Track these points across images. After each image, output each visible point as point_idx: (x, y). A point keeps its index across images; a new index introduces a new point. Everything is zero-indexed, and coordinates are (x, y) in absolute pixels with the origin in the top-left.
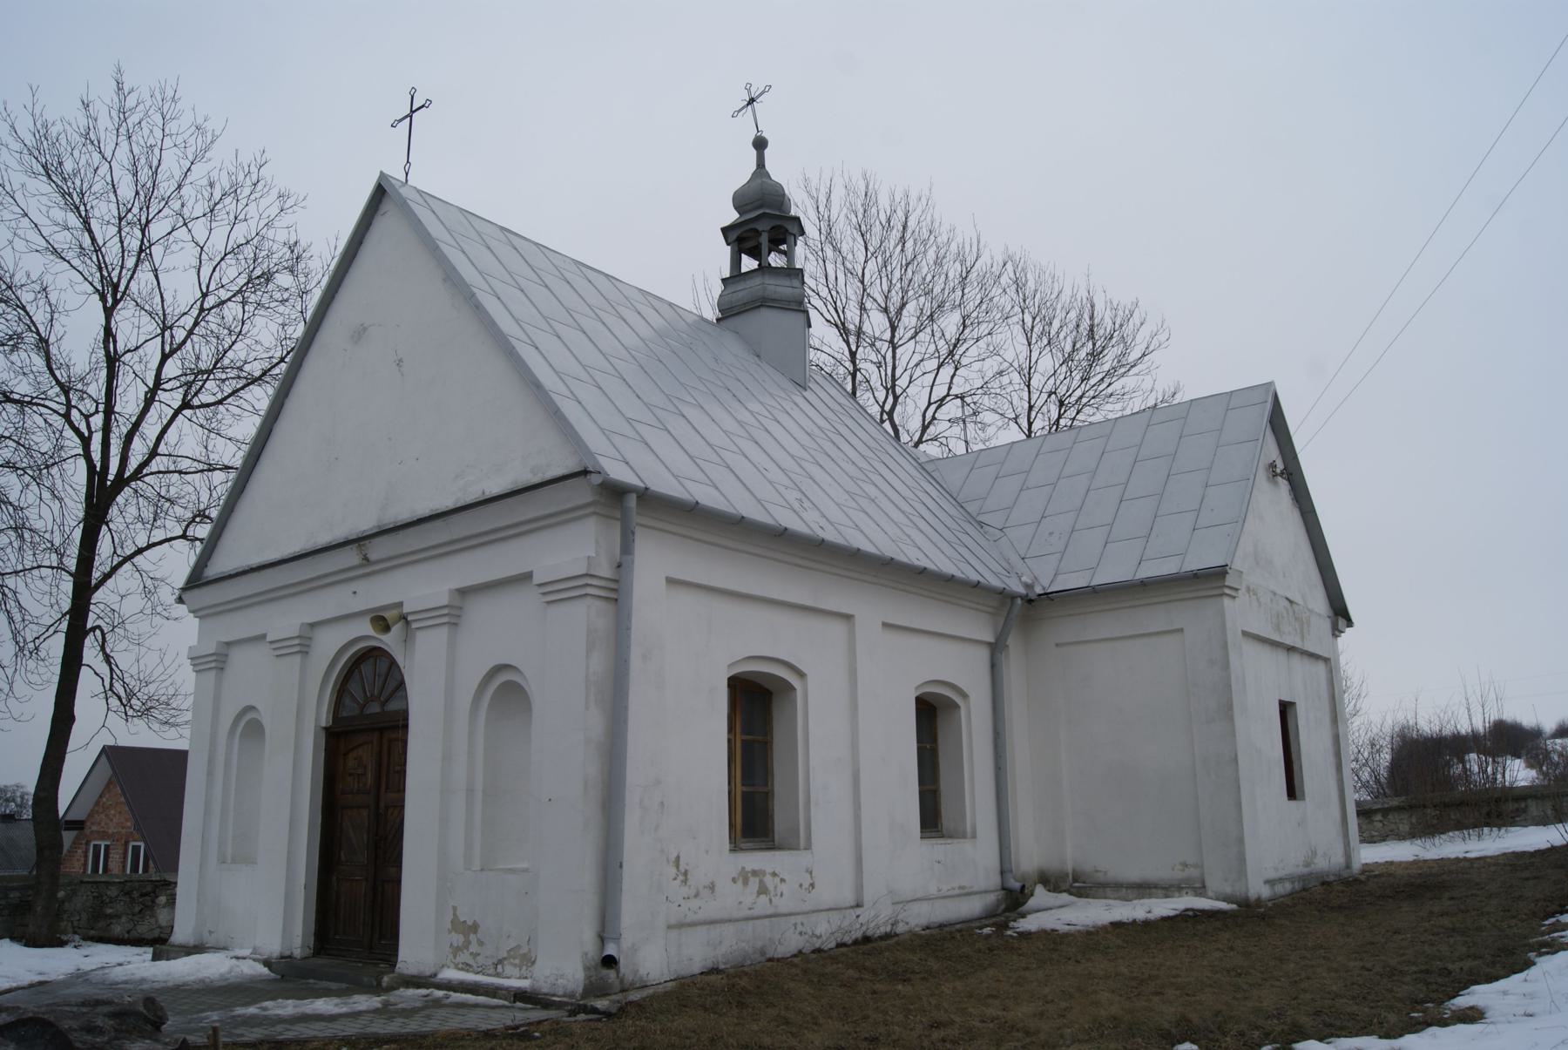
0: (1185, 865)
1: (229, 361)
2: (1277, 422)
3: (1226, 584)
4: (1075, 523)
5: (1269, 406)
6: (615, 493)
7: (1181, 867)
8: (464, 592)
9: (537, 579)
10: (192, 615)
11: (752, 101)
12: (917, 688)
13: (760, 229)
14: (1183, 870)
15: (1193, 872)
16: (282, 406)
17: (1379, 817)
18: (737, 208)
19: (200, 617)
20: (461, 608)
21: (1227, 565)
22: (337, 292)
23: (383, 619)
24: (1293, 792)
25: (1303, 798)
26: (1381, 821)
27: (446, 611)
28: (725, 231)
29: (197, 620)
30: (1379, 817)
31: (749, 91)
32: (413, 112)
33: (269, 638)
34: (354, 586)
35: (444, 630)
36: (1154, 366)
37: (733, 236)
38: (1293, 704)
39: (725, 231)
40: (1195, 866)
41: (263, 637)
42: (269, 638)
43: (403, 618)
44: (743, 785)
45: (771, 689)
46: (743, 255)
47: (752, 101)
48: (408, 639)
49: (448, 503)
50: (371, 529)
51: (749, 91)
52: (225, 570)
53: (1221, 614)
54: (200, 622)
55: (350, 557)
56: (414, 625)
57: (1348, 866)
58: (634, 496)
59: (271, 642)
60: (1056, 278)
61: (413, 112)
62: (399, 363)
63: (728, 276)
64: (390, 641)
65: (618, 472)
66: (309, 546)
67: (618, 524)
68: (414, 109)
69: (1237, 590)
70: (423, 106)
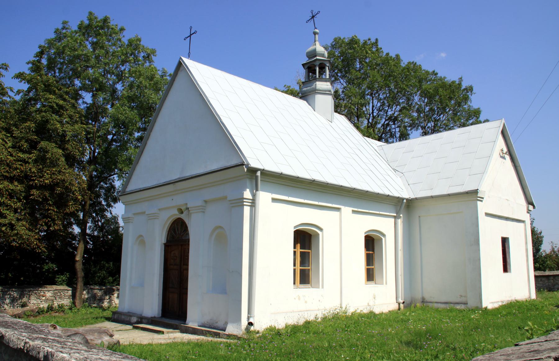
0: (461, 296)
3: (478, 196)
4: (130, 330)
7: (460, 297)
10: (122, 204)
11: (313, 17)
12: (365, 233)
13: (315, 64)
14: (460, 298)
15: (463, 300)
17: (552, 278)
18: (307, 56)
19: (125, 205)
20: (205, 206)
21: (478, 189)
22: (166, 97)
23: (181, 209)
24: (506, 268)
25: (510, 272)
26: (552, 279)
27: (201, 207)
28: (303, 65)
29: (124, 205)
30: (552, 278)
31: (312, 13)
32: (191, 35)
33: (146, 213)
37: (306, 66)
38: (508, 238)
39: (303, 65)
40: (465, 297)
41: (144, 213)
42: (146, 213)
43: (188, 209)
44: (300, 266)
45: (311, 234)
47: (313, 17)
48: (189, 215)
51: (312, 13)
53: (476, 207)
54: (125, 207)
56: (191, 212)
57: (530, 297)
59: (147, 215)
61: (190, 36)
63: (304, 81)
64: (183, 216)
65: (254, 164)
68: (191, 34)
69: (483, 198)
70: (194, 33)
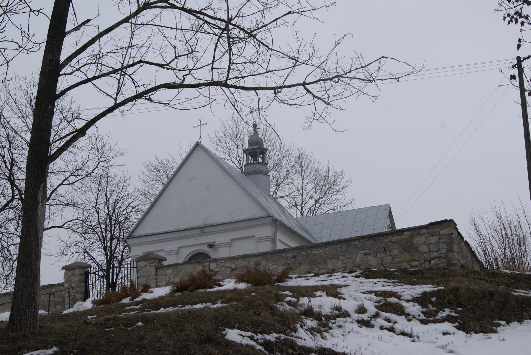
1: (52, 170)
2: (390, 216)
5: (389, 210)
6: (275, 221)
8: (232, 240)
9: (256, 237)
16: (162, 193)
34: (196, 238)
35: (228, 248)
36: (346, 192)
46: (58, 93)
49: (228, 220)
50: (202, 225)
52: (141, 234)
55: (198, 231)
58: (278, 222)
59: (165, 251)
60: (313, 158)
62: (207, 188)
66: (177, 228)
67: (274, 228)
